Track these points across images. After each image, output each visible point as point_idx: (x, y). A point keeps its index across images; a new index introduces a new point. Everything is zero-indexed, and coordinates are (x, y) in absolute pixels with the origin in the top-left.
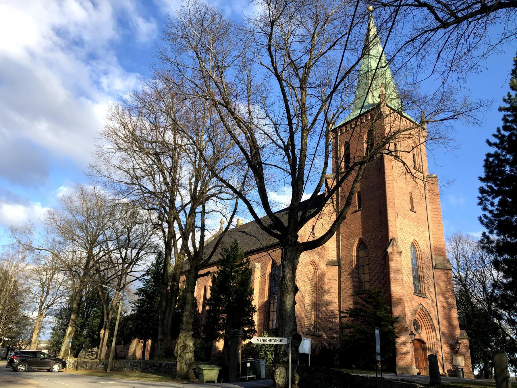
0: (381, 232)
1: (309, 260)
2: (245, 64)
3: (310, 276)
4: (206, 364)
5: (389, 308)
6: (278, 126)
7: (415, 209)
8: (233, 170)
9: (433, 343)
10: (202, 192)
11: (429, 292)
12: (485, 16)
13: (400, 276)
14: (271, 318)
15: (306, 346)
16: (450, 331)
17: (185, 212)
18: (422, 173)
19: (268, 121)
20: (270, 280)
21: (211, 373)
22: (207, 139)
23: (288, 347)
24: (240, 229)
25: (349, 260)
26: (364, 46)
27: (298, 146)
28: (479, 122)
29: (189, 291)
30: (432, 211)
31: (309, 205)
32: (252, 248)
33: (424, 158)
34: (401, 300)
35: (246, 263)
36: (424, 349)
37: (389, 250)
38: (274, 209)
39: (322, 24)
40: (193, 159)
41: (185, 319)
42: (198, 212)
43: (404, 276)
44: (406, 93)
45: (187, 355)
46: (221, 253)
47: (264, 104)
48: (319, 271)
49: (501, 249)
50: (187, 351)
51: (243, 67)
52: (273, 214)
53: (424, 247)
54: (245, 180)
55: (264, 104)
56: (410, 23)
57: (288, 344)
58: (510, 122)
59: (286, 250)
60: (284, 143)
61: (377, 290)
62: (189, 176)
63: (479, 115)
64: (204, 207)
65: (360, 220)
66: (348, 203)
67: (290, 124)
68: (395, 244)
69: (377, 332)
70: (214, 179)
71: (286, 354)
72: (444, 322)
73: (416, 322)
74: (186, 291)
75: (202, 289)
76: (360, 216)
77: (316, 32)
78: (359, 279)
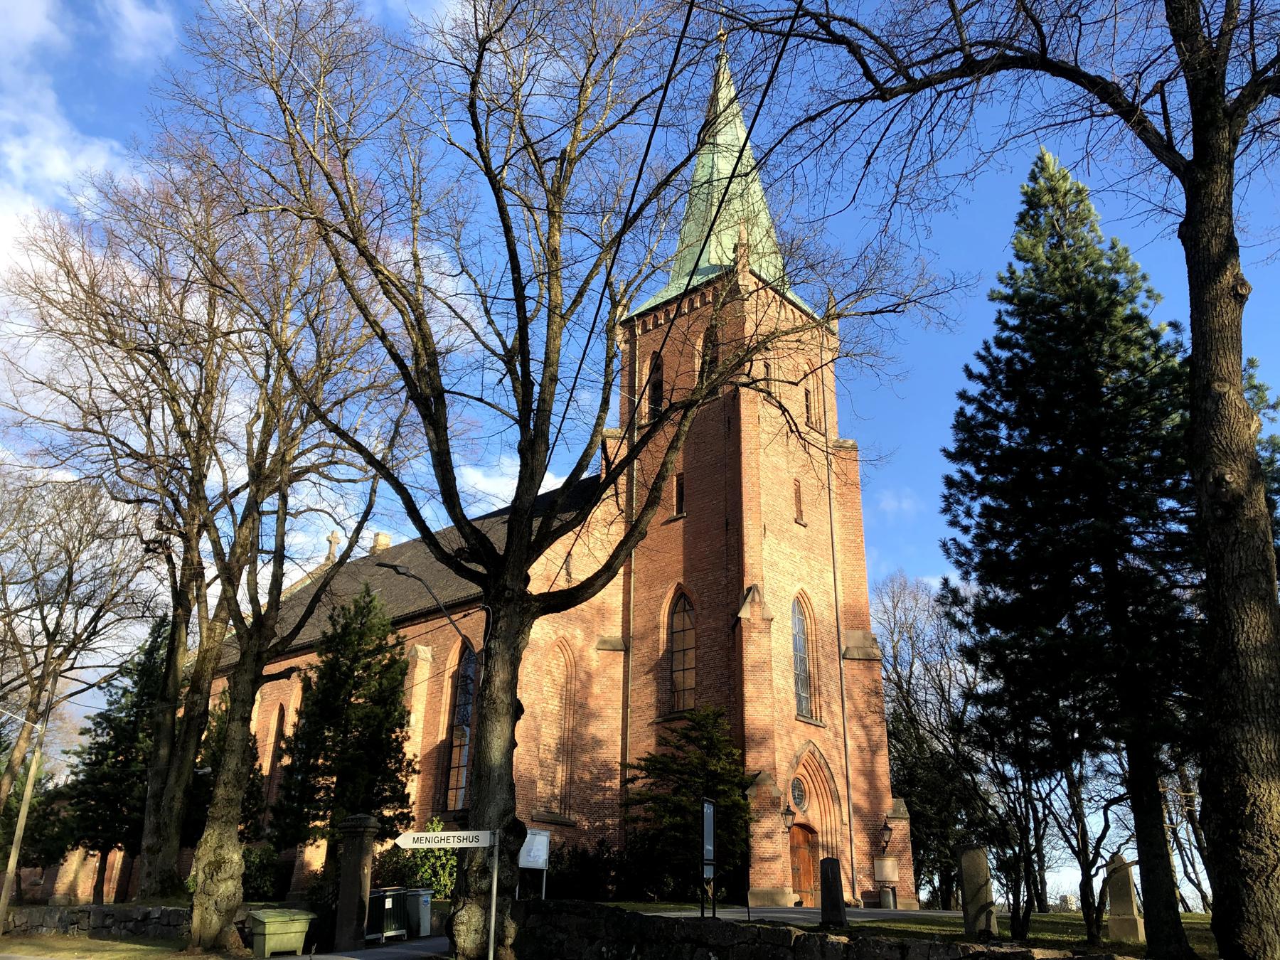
0: (728, 570)
1: (554, 638)
2: (407, 134)
4: (274, 908)
5: (737, 752)
7: (805, 520)
10: (281, 459)
11: (831, 713)
14: (452, 783)
15: (536, 851)
16: (871, 803)
17: (232, 510)
19: (463, 283)
20: (455, 688)
24: (381, 561)
27: (537, 350)
28: (950, 323)
29: (237, 717)
32: (411, 609)
33: (831, 399)
35: (394, 646)
36: (814, 846)
37: (745, 613)
39: (605, 55)
40: (261, 372)
41: (220, 792)
42: (268, 513)
50: (222, 875)
51: (400, 143)
52: (469, 523)
53: (821, 605)
57: (492, 847)
58: (1015, 329)
62: (248, 416)
63: (950, 305)
64: (284, 499)
65: (681, 541)
66: (653, 501)
67: (520, 299)
68: (757, 599)
69: (708, 810)
70: (318, 425)
71: (485, 872)
72: (860, 782)
73: (797, 786)
75: (276, 710)
76: (681, 531)
78: (673, 683)
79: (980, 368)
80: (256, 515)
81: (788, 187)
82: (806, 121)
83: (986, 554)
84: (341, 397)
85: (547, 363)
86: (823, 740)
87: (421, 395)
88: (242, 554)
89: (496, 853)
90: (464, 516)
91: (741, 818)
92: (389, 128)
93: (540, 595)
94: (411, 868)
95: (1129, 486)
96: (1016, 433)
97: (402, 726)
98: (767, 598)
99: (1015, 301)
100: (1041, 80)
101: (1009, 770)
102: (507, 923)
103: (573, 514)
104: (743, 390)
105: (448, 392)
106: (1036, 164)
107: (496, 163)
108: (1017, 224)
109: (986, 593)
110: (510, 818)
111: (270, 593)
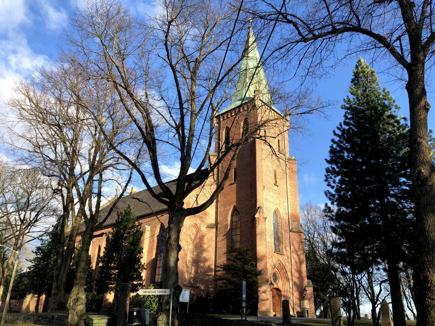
1: (192, 223)
2: (144, 53)
3: (193, 237)
4: (96, 315)
7: (278, 184)
9: (287, 291)
10: (100, 162)
11: (286, 250)
14: (157, 273)
15: (185, 296)
17: (83, 179)
20: (158, 240)
22: (107, 115)
23: (170, 297)
25: (225, 224)
28: (328, 117)
29: (85, 249)
30: (291, 186)
32: (144, 213)
33: (287, 143)
35: (138, 226)
36: (280, 296)
37: (257, 216)
39: (211, 27)
40: (94, 132)
41: (78, 275)
42: (96, 180)
45: (79, 307)
48: (200, 232)
50: (79, 303)
52: (163, 184)
53: (283, 214)
54: (139, 153)
57: (170, 295)
61: (246, 248)
64: (101, 176)
65: (235, 191)
66: (226, 177)
67: (181, 108)
68: (261, 211)
69: (244, 283)
70: (113, 151)
71: (168, 303)
72: (296, 274)
73: (275, 275)
75: (97, 247)
78: (232, 239)
80: (91, 181)
84: (121, 141)
85: (191, 130)
86: (283, 259)
87: (148, 141)
88: (87, 194)
89: (172, 297)
91: (256, 286)
95: (389, 173)
96: (350, 155)
97: (140, 253)
98: (265, 211)
102: (175, 321)
103: (199, 181)
104: (257, 140)
105: (157, 140)
106: (358, 63)
107: (174, 63)
108: (352, 82)
111: (96, 207)
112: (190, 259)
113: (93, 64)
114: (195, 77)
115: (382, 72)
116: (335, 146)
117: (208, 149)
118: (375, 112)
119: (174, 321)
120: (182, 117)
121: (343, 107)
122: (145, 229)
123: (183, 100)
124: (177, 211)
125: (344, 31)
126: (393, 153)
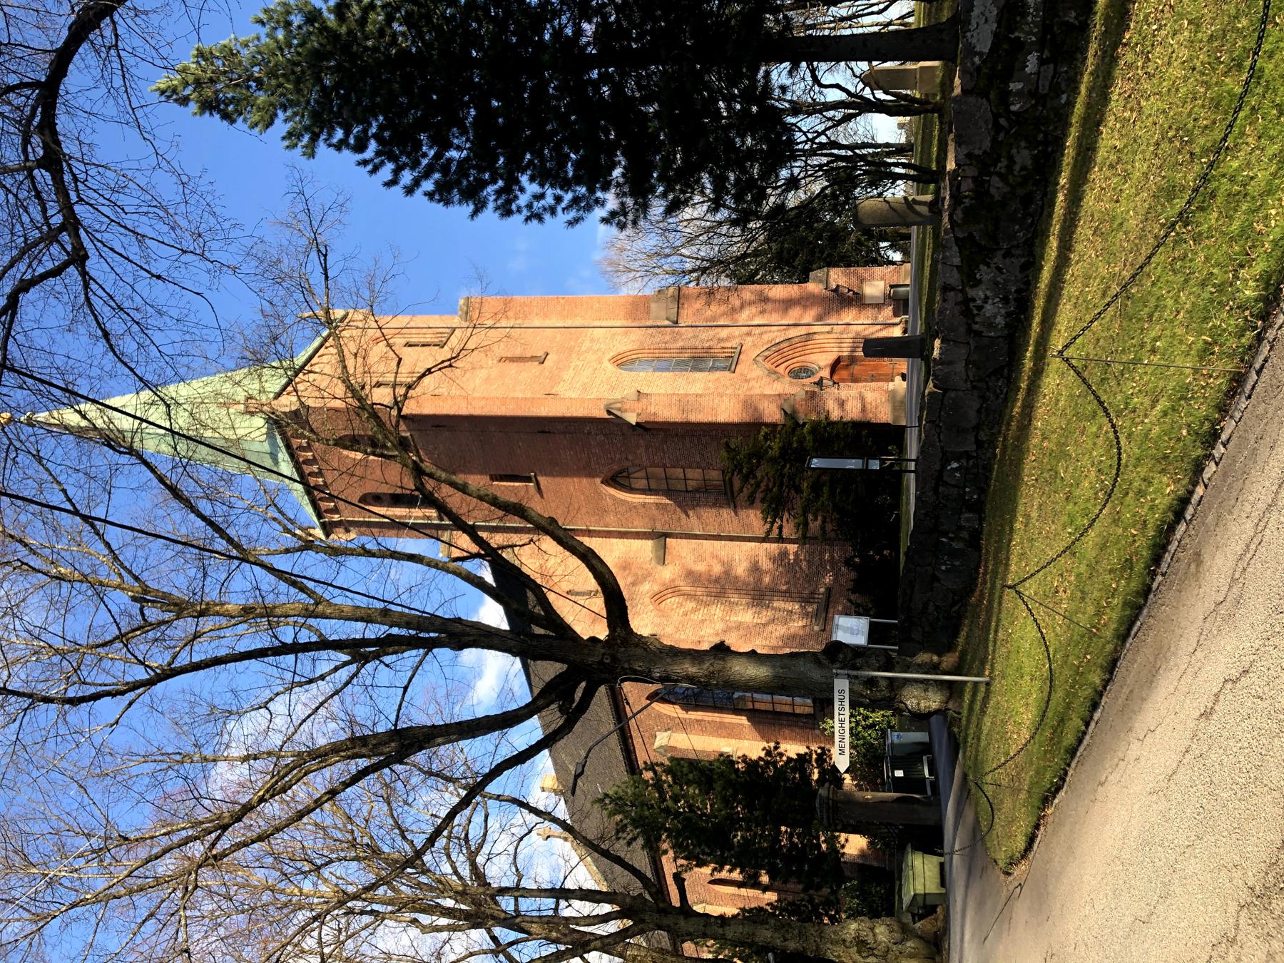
0: (589, 433)
1: (651, 607)
2: (106, 769)
3: (691, 605)
4: (901, 885)
5: (764, 430)
6: (297, 679)
7: (541, 353)
8: (406, 803)
9: (840, 342)
10: (461, 895)
11: (728, 339)
12: (69, 165)
13: (692, 399)
14: (788, 709)
15: (852, 630)
16: (812, 304)
17: (511, 944)
18: (454, 329)
19: (279, 706)
20: (697, 707)
21: (921, 874)
22: (313, 877)
23: (856, 677)
24: (570, 788)
25: (654, 511)
26: (106, 448)
27: (356, 630)
28: (341, 200)
29: (720, 931)
30: (546, 316)
31: (515, 606)
32: (619, 753)
33: (420, 321)
34: (745, 402)
35: (655, 772)
36: (853, 360)
37: (632, 419)
38: (523, 696)
39: (23, 552)
40: (367, 919)
41: (792, 945)
42: (516, 905)
43: (692, 391)
44: (248, 354)
45: (881, 938)
46: (629, 844)
47: (230, 713)
48: (677, 583)
49: (639, 189)
50: (870, 939)
51: (117, 778)
52: (535, 700)
53: (626, 342)
54: (437, 775)
55: (230, 713)
56: (58, 337)
57: (849, 676)
58: (347, 134)
59: (624, 671)
60: (345, 664)
61: (724, 454)
62: (414, 932)
63: (321, 199)
64: (503, 891)
65: (559, 480)
66: (518, 510)
67: (296, 648)
68: (619, 405)
69: (816, 463)
70: (427, 858)
71: (872, 682)
72: (794, 314)
73: (796, 374)
74: (722, 940)
75: (717, 895)
76: (550, 479)
77: (44, 568)
78: (697, 490)
79: (387, 171)
80: (518, 920)
81: (185, 360)
82: (108, 341)
83: (578, 180)
84: (397, 831)
85: (368, 619)
86: (753, 347)
87: (397, 752)
88: (558, 931)
89: (855, 673)
90: (527, 705)
91: (825, 428)
92: (96, 790)
93: (609, 626)
94: (867, 750)
95: (514, 34)
96: (456, 141)
97: (732, 763)
98: (618, 396)
99: (317, 130)
100: (71, 89)
101: (784, 173)
102: (919, 661)
103: (529, 594)
104: (405, 411)
105: (396, 725)
106: (169, 97)
107: (141, 674)
108: (233, 122)
109: (618, 185)
110: (822, 658)
111: (598, 902)
112: (750, 612)
113: (138, 940)
114: (193, 605)
115: (198, 30)
116: (428, 185)
117: (429, 565)
118: (328, 60)
119: (919, 665)
120: (325, 644)
121: (310, 152)
122: (667, 748)
123: (267, 645)
124: (614, 658)
125: (54, 133)
126: (453, 16)
